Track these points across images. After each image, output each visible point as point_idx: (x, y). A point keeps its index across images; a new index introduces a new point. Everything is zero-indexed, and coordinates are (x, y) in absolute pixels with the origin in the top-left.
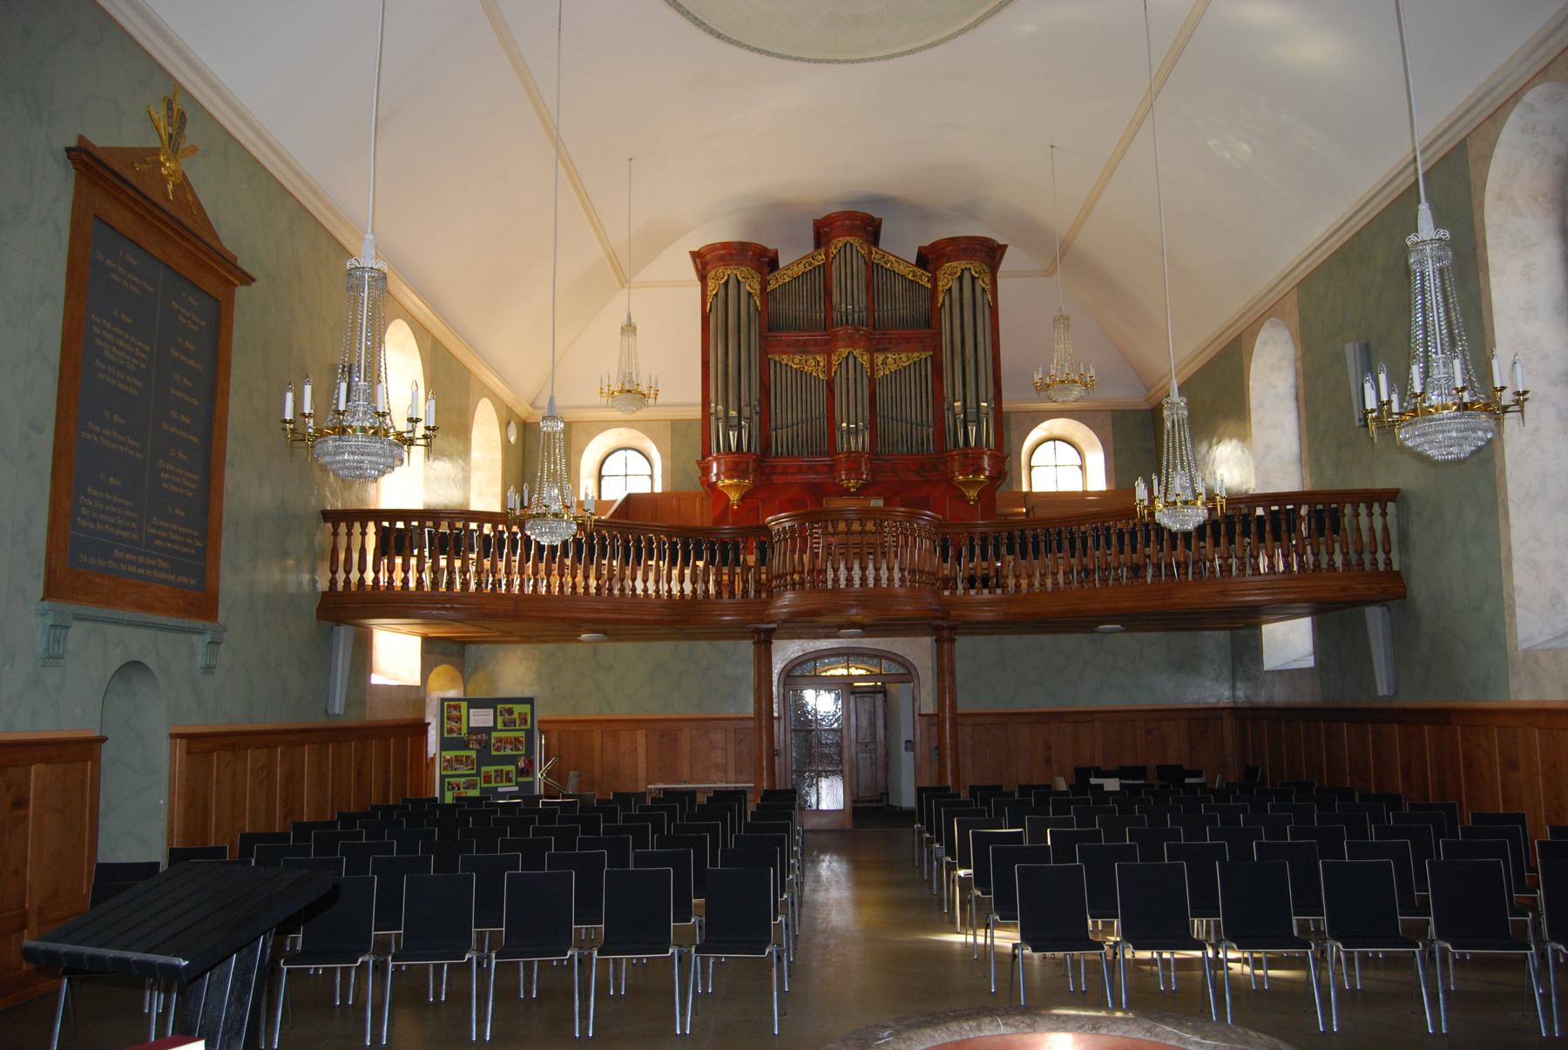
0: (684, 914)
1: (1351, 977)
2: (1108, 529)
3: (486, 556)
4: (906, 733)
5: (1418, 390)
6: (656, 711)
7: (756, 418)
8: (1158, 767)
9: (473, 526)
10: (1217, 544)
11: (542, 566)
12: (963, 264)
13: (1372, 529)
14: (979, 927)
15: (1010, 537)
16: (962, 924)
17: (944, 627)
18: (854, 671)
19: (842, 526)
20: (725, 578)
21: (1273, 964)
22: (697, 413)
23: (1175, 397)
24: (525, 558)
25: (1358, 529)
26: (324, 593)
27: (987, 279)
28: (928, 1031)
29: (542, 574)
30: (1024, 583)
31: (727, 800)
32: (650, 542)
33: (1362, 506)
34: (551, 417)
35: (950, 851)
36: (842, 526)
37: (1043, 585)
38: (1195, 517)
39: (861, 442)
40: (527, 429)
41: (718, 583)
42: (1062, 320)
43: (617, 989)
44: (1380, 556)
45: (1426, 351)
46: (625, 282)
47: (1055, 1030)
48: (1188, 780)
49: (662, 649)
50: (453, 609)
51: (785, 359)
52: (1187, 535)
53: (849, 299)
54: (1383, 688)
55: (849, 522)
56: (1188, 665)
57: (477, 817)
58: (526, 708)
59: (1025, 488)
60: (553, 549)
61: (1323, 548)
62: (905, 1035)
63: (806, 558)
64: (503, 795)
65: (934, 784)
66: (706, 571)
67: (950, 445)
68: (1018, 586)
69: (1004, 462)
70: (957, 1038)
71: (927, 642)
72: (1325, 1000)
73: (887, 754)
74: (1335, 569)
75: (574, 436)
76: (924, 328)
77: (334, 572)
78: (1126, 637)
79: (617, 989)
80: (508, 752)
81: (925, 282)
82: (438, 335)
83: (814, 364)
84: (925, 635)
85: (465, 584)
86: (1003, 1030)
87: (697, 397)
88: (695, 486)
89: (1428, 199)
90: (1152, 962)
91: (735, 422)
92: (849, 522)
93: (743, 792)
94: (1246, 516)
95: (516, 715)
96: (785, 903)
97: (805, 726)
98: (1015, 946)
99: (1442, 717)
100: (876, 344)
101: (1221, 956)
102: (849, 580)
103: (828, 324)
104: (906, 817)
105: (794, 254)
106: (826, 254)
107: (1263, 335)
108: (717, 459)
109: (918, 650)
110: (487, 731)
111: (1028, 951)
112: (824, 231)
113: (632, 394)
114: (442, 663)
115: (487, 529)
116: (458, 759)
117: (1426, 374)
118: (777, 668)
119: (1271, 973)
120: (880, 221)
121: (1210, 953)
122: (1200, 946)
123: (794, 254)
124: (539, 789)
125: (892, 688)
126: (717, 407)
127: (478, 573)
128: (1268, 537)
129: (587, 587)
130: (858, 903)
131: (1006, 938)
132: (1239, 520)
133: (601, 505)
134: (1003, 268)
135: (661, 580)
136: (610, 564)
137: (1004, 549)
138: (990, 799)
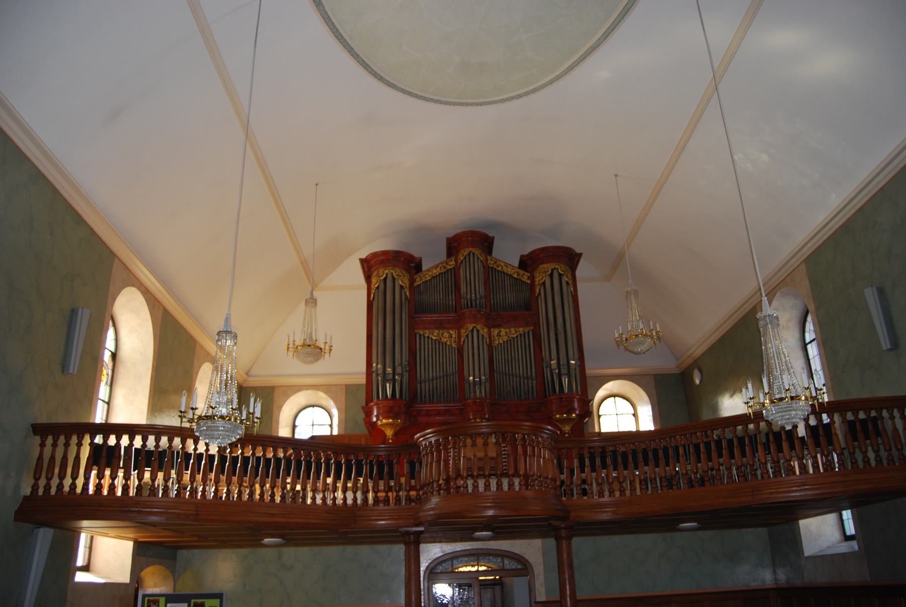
7: (406, 375)
12: (553, 266)
22: (362, 380)
26: (25, 498)
27: (569, 276)
53: (473, 287)
59: (597, 430)
76: (526, 310)
77: (37, 479)
83: (448, 337)
87: (363, 369)
88: (363, 430)
91: (391, 377)
105: (433, 261)
106: (456, 261)
109: (532, 549)
112: (454, 244)
113: (312, 350)
114: (153, 564)
120: (493, 239)
125: (507, 580)
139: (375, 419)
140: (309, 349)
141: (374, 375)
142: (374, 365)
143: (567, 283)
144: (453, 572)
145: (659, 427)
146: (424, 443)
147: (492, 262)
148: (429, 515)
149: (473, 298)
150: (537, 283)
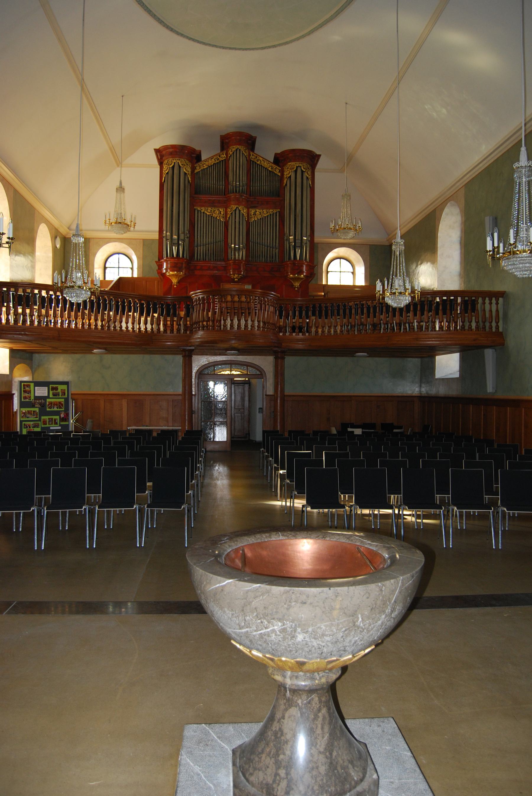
0: (142, 489)
1: (461, 523)
2: (363, 305)
3: (43, 308)
4: (259, 405)
5: (512, 242)
6: (133, 390)
7: (187, 240)
8: (382, 424)
9: (36, 291)
10: (415, 315)
11: (73, 314)
12: (298, 164)
13: (491, 311)
14: (288, 498)
15: (314, 307)
16: (281, 496)
17: (279, 352)
18: (234, 372)
19: (229, 298)
20: (169, 323)
21: (426, 517)
22: (156, 236)
23: (399, 239)
24: (64, 309)
25: (484, 310)
27: (309, 173)
28: (246, 538)
29: (73, 317)
30: (320, 330)
31: (166, 435)
32: (130, 303)
33: (487, 299)
34: (77, 235)
35: (276, 462)
36: (229, 298)
37: (329, 332)
38: (406, 300)
39: (241, 255)
40: (66, 241)
41: (165, 325)
42: (347, 196)
43: (109, 525)
44: (494, 324)
45: (518, 223)
46: (119, 163)
47: (306, 538)
48: (395, 431)
49: (136, 359)
50: (26, 335)
51: (203, 209)
52: (401, 309)
53: (238, 179)
54: (490, 388)
55: (233, 296)
56: (398, 375)
57: (39, 441)
58: (65, 387)
59: (324, 283)
60: (79, 305)
61: (466, 319)
62: (235, 539)
63: (210, 314)
64: (53, 431)
65: (272, 429)
66: (158, 319)
67: (286, 259)
68: (317, 332)
69: (314, 268)
70: (259, 541)
71: (271, 359)
72: (447, 533)
73: (249, 415)
74: (472, 330)
75: (89, 247)
76: (275, 196)
78: (370, 359)
79: (109, 525)
80: (56, 409)
81: (277, 172)
82: (18, 188)
83: (218, 213)
84: (270, 355)
85: (32, 322)
86: (281, 537)
89: (525, 146)
90: (369, 515)
91: (176, 242)
92: (233, 296)
93: (176, 431)
94: (431, 301)
95: (59, 390)
96: (193, 486)
97: (209, 401)
98: (303, 506)
99: (516, 403)
100: (250, 205)
101: (401, 513)
102: (232, 326)
103: (226, 192)
104: (257, 445)
105: (209, 154)
106: (227, 154)
107: (446, 210)
108: (166, 261)
109: (266, 363)
110: (44, 398)
111: (309, 509)
112: (226, 141)
113: (122, 224)
115: (44, 293)
116: (29, 412)
117: (517, 233)
118: (195, 370)
119: (424, 521)
121: (397, 512)
122: (391, 507)
123: (209, 154)
124: (71, 428)
125: (253, 381)
126: (167, 234)
127: (39, 316)
128: (440, 312)
129: (96, 325)
130: (232, 486)
131: (299, 503)
132: (427, 303)
133: (104, 282)
134: (318, 166)
135: (134, 323)
136: (109, 314)
137: (310, 313)
138: (299, 437)
139: (164, 271)
140: (120, 225)
141: (164, 239)
142: (165, 232)
143: (307, 178)
144: (214, 374)
145: (368, 284)
146: (195, 297)
147: (254, 157)
148: (197, 342)
149: (238, 186)
150: (285, 176)
